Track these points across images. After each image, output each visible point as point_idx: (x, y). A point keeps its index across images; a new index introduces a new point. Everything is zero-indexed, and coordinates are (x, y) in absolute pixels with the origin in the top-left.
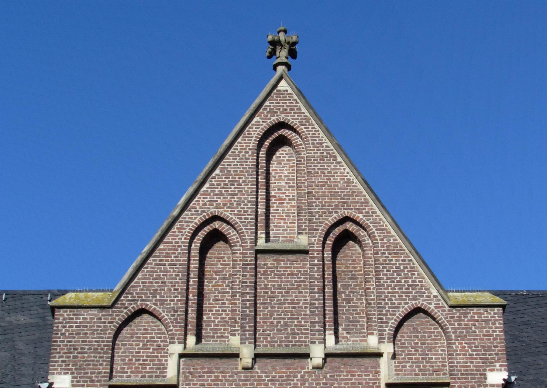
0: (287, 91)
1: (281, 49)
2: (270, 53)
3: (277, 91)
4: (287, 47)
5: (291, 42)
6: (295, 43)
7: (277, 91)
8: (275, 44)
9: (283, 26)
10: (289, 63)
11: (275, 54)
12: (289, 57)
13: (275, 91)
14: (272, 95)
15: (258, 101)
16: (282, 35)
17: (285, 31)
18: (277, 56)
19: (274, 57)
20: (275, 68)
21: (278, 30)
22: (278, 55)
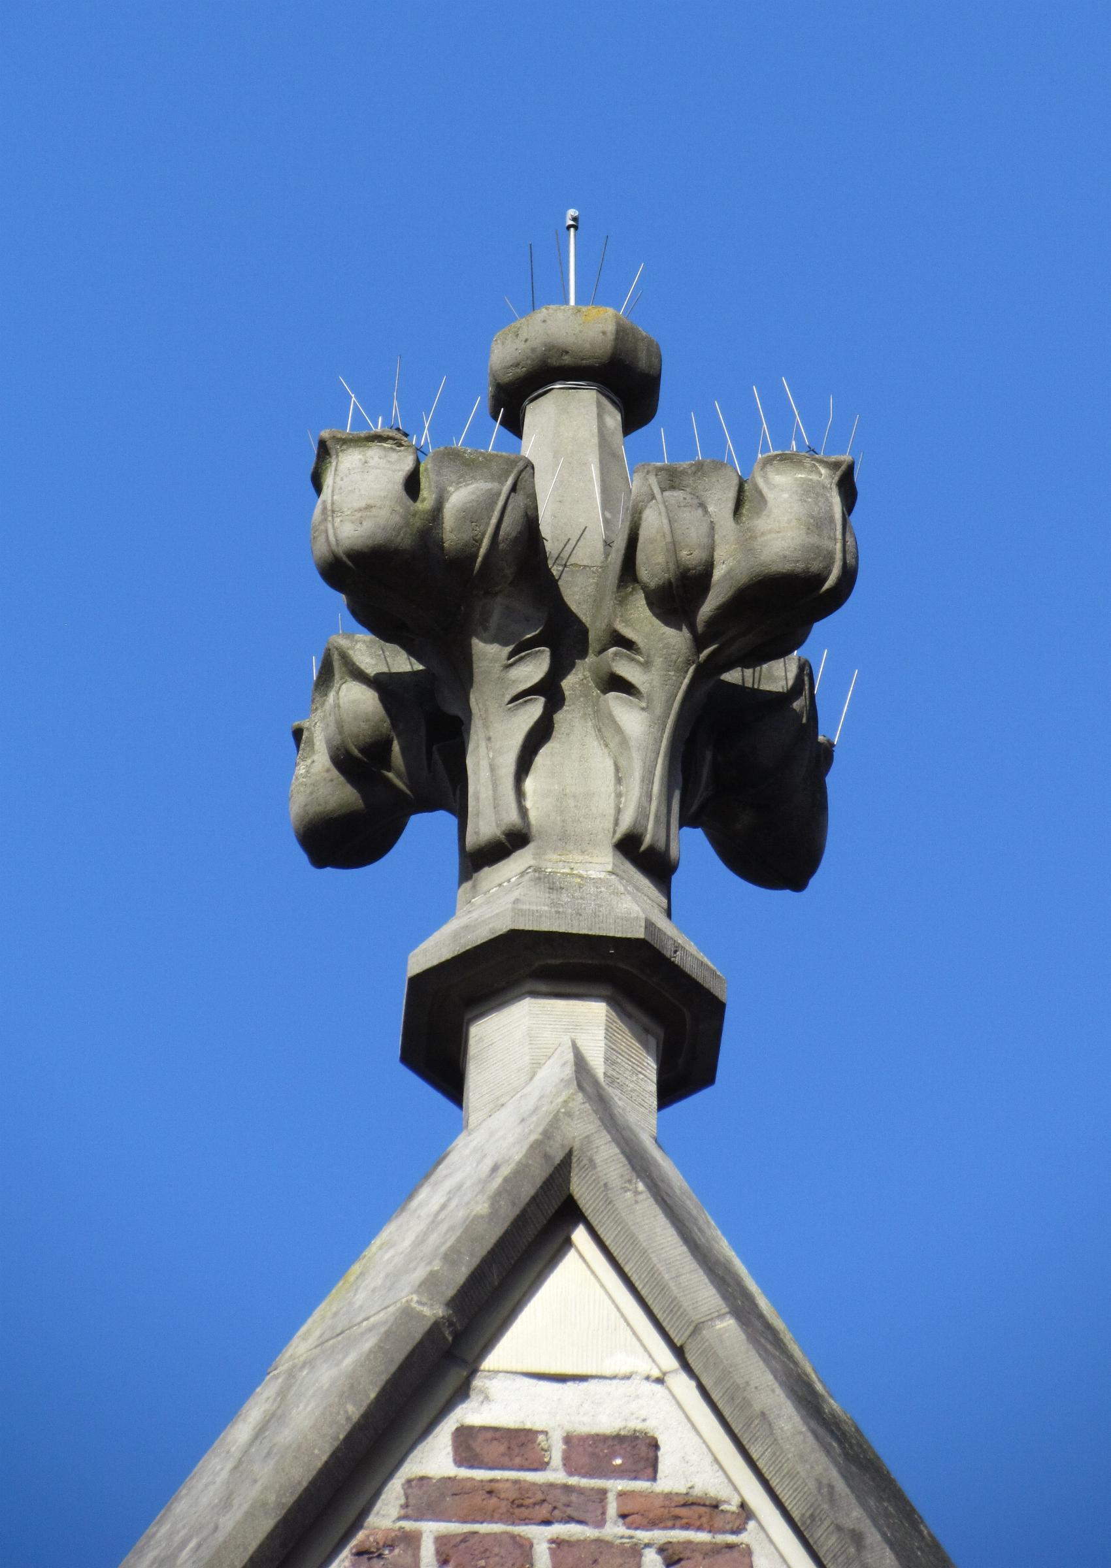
0: (641, 1452)
1: (550, 691)
2: (358, 762)
3: (468, 1445)
4: (661, 655)
5: (728, 571)
6: (787, 604)
7: (468, 1445)
8: (442, 596)
9: (589, 295)
10: (690, 950)
11: (448, 789)
12: (693, 849)
13: (434, 1458)
14: (386, 1514)
15: (494, 521)
16: (566, 431)
17: (628, 384)
18: (485, 825)
19: (426, 834)
20: (435, 1034)
21: (507, 351)
22: (489, 810)
